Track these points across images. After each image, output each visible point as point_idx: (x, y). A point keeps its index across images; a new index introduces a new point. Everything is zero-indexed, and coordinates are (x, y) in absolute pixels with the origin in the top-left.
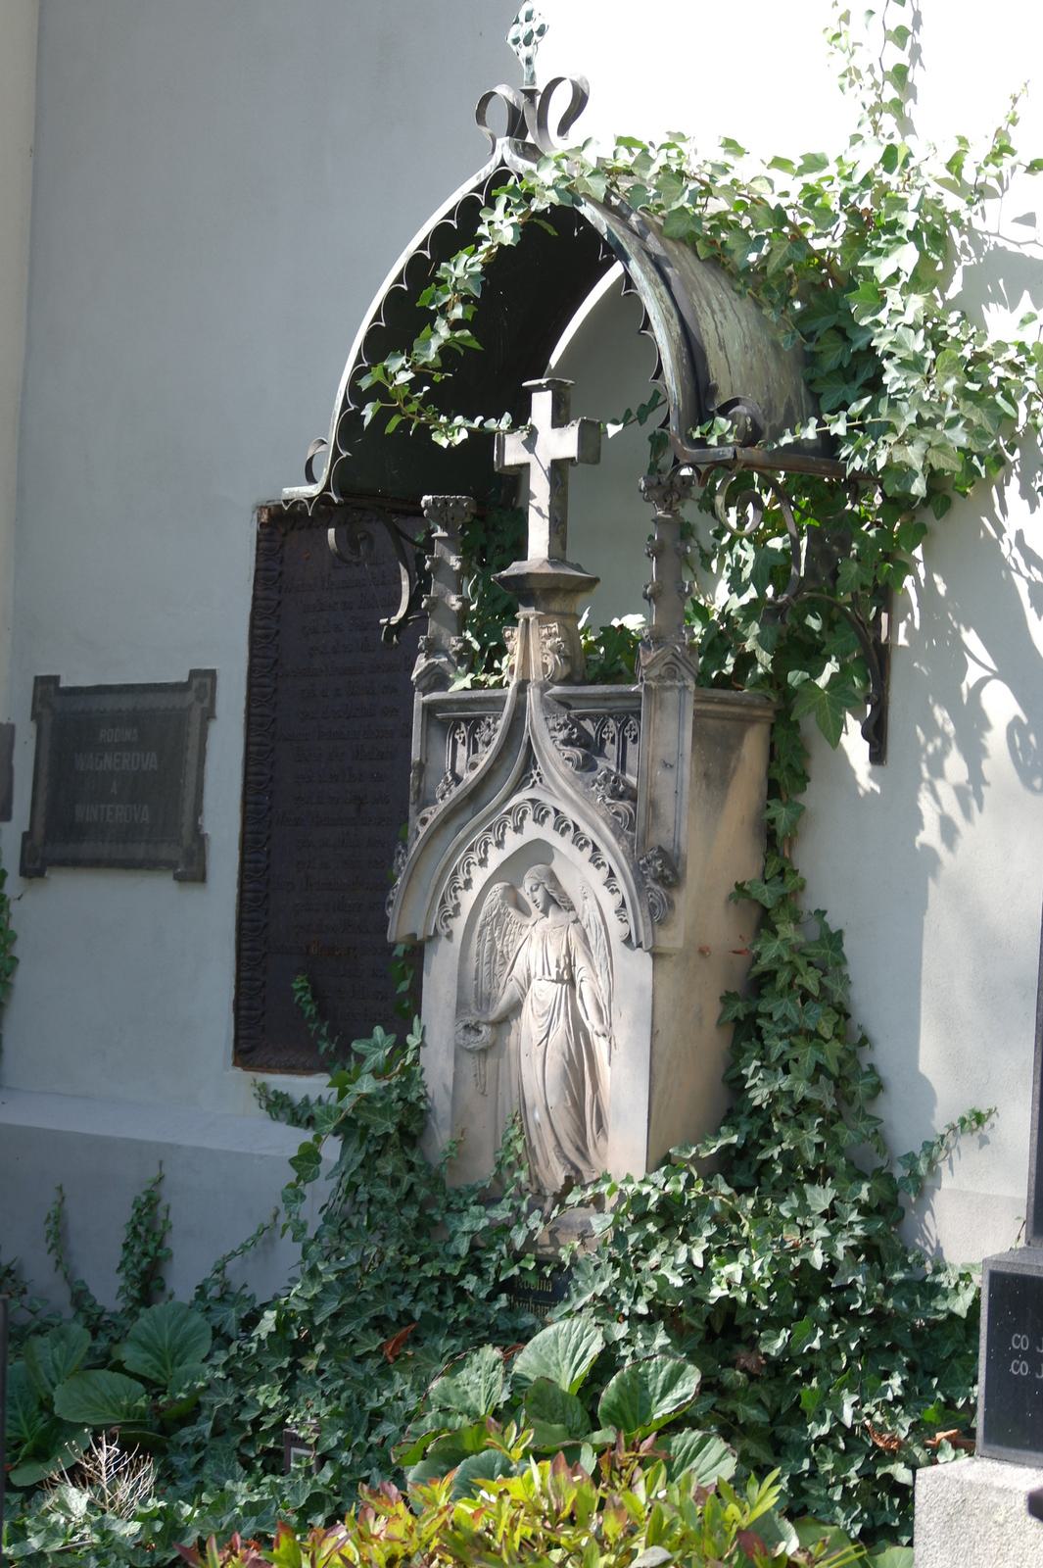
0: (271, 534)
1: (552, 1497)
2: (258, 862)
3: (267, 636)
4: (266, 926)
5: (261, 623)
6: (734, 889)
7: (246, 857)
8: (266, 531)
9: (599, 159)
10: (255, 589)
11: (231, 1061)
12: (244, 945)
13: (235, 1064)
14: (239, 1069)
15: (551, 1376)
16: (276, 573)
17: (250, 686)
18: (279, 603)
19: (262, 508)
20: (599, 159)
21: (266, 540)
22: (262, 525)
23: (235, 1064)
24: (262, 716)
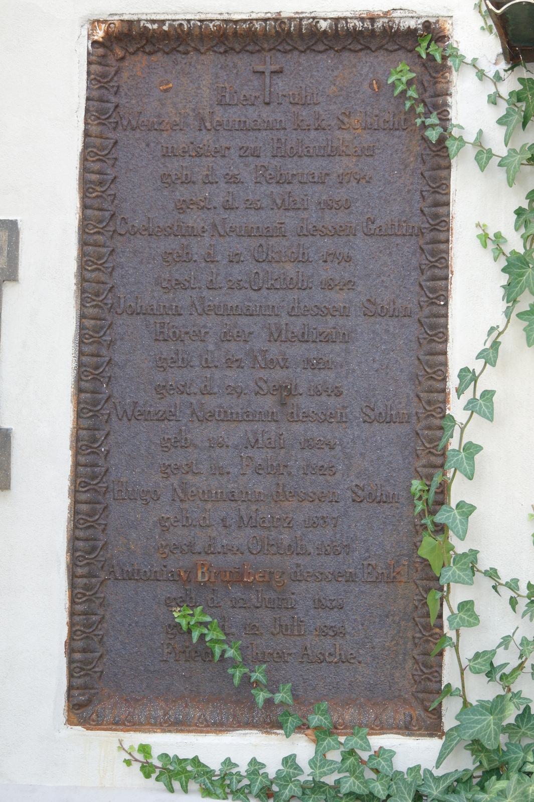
0: (104, 56)
1: (525, 786)
2: (96, 465)
3: (101, 183)
4: (114, 180)
5: (96, 166)
6: (449, 117)
7: (82, 460)
8: (101, 51)
9: (253, 762)
10: (86, 123)
11: (63, 719)
12: (80, 571)
13: (70, 722)
14: (79, 728)
15: (503, 65)
16: (107, 214)
17: (83, 243)
18: (116, 143)
19: (95, 23)
20: (253, 762)
21: (100, 64)
22: (95, 43)
23: (70, 722)
24: (98, 282)
